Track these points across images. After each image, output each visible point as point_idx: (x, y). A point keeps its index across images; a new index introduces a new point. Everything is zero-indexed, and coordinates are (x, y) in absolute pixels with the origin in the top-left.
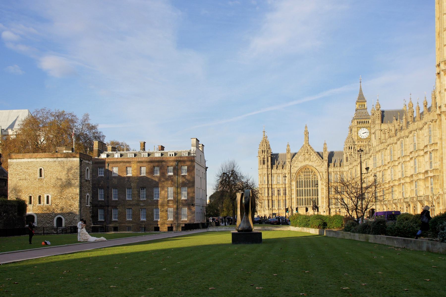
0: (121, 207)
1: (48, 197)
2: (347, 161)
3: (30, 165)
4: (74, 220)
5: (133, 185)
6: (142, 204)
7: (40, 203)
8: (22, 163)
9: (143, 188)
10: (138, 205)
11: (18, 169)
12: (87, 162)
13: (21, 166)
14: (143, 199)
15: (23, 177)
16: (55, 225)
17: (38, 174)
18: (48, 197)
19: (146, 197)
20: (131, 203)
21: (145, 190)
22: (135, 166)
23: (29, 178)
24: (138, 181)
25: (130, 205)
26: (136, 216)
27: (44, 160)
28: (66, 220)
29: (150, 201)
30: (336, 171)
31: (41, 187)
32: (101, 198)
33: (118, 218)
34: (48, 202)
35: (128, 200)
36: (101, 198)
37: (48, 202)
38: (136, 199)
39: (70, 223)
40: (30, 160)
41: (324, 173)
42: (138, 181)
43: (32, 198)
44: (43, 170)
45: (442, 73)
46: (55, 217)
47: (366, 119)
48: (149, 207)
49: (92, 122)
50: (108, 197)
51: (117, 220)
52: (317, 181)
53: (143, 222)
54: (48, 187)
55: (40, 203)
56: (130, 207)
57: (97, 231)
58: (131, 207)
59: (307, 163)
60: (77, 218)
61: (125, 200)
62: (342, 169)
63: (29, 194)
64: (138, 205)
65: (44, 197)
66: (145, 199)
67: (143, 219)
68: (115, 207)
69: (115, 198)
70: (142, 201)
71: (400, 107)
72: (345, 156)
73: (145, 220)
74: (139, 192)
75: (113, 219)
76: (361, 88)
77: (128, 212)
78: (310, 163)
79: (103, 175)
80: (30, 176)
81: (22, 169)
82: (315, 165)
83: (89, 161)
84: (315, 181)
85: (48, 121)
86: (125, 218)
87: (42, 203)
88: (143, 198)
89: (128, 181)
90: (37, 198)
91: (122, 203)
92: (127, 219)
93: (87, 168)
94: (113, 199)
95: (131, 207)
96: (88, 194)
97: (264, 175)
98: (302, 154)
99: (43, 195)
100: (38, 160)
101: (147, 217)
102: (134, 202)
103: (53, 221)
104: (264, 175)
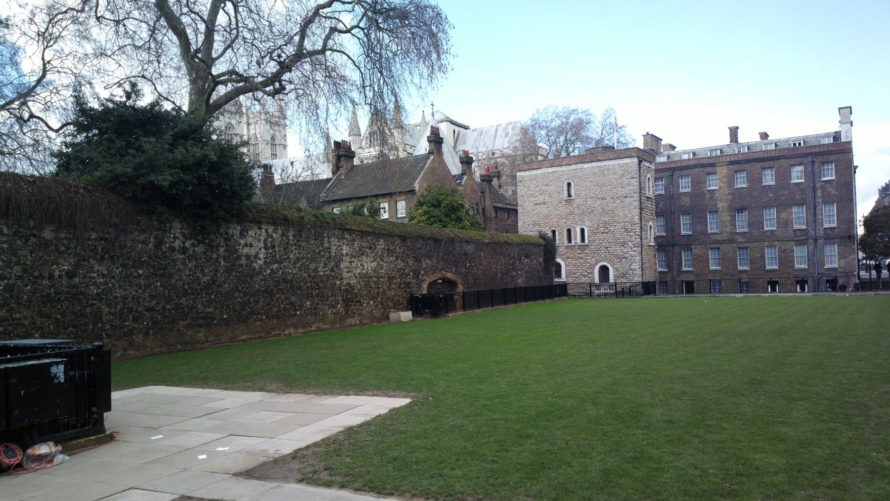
0: (698, 246)
1: (582, 230)
3: (551, 179)
5: (720, 205)
7: (570, 241)
8: (536, 176)
9: (740, 210)
10: (731, 241)
11: (532, 186)
12: (648, 165)
15: (540, 199)
16: (597, 280)
17: (566, 192)
18: (582, 230)
19: (749, 226)
20: (719, 238)
21: (746, 213)
24: (730, 197)
25: (716, 242)
27: (574, 167)
28: (616, 269)
29: (756, 233)
31: (571, 213)
33: (694, 266)
34: (583, 240)
37: (583, 240)
38: (728, 230)
39: (624, 275)
40: (550, 170)
42: (730, 197)
43: (557, 233)
48: (755, 244)
50: (673, 230)
53: (742, 272)
55: (570, 241)
56: (716, 246)
57: (654, 292)
58: (719, 246)
61: (705, 233)
64: (731, 241)
66: (746, 230)
67: (771, 265)
68: (687, 247)
69: (798, 178)
70: (740, 234)
73: (746, 268)
74: (733, 218)
75: (684, 269)
77: (712, 255)
79: (663, 192)
80: (550, 196)
83: (651, 163)
85: (553, 125)
86: (708, 266)
87: (573, 241)
88: (742, 224)
89: (711, 198)
90: (565, 233)
91: (700, 238)
92: (711, 268)
93: (649, 176)
94: (683, 232)
95: (719, 246)
96: (651, 223)
99: (574, 228)
100: (564, 168)
101: (752, 262)
102: (725, 236)
103: (592, 273)
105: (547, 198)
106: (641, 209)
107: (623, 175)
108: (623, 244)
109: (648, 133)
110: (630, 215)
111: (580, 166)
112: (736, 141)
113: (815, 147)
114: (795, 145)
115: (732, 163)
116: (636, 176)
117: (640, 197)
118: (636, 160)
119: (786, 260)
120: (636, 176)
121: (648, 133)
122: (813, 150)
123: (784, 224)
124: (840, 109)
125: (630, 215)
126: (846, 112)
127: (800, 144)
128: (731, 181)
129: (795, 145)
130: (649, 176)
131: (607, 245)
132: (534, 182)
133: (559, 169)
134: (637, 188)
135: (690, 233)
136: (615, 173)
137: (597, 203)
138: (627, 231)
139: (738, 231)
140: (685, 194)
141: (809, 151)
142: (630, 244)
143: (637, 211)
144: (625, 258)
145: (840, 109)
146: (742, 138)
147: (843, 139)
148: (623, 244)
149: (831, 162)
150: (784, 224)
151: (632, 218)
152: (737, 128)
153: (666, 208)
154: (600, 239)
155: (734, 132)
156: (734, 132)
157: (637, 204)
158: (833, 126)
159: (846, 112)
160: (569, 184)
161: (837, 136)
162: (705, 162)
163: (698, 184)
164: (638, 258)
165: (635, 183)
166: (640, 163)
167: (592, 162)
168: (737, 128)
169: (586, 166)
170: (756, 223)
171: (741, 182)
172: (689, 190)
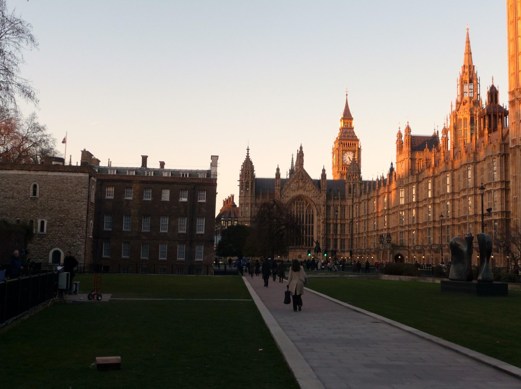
1: (43, 223)
2: (350, 192)
4: (77, 254)
5: (132, 211)
6: (144, 238)
8: (8, 175)
13: (8, 180)
14: (145, 230)
17: (32, 192)
22: (138, 187)
23: (18, 196)
26: (172, 254)
27: (40, 173)
30: (337, 205)
31: (35, 208)
32: (106, 228)
35: (125, 232)
36: (106, 228)
40: (20, 172)
41: (322, 207)
44: (38, 186)
45: (517, 102)
46: (51, 249)
47: (353, 140)
49: (41, 121)
51: (108, 256)
52: (313, 215)
53: (125, 259)
54: (43, 210)
59: (301, 192)
60: (81, 253)
62: (343, 203)
63: (16, 217)
65: (37, 223)
66: (148, 231)
67: (144, 257)
70: (144, 233)
71: (429, 133)
72: (347, 187)
74: (141, 221)
75: (104, 256)
76: (347, 100)
78: (305, 193)
80: (19, 193)
81: (8, 183)
82: (310, 195)
84: (310, 215)
88: (146, 227)
94: (105, 229)
97: (247, 204)
98: (295, 181)
100: (32, 173)
103: (48, 256)
104: (247, 204)
105: (15, 194)
106: (88, 211)
107: (77, 185)
108: (73, 236)
109: (85, 150)
110: (80, 215)
111: (45, 173)
112: (146, 166)
113: (195, 179)
114: (183, 175)
115: (143, 182)
116: (87, 186)
117: (88, 202)
118: (87, 175)
119: (172, 254)
120: (87, 186)
121: (85, 150)
122: (194, 181)
123: (173, 228)
124: (212, 156)
125: (80, 215)
126: (215, 159)
127: (186, 175)
128: (141, 195)
129: (183, 175)
130: (93, 187)
131: (61, 235)
132: (6, 180)
133: (27, 173)
134: (87, 195)
135: (110, 229)
136: (71, 182)
137: (56, 203)
138: (77, 227)
139: (143, 231)
140: (109, 200)
141: (192, 181)
142: (79, 236)
143: (85, 212)
144: (74, 246)
145: (212, 156)
146: (149, 165)
147: (212, 177)
148: (73, 236)
149: (204, 191)
150: (173, 228)
151: (82, 217)
152: (147, 157)
153: (100, 209)
154: (56, 231)
155: (144, 159)
156: (144, 159)
157: (85, 207)
158: (206, 166)
159: (215, 159)
160: (35, 186)
161: (208, 173)
162: (125, 178)
163: (119, 194)
164: (83, 247)
165: (85, 191)
166: (90, 177)
167: (55, 171)
168: (147, 157)
169: (50, 174)
170: (155, 227)
171: (148, 198)
172: (112, 197)
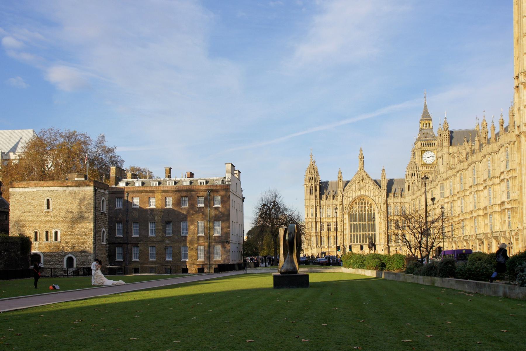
0: (143, 245)
1: (56, 233)
2: (409, 190)
3: (35, 195)
4: (87, 259)
5: (156, 218)
6: (167, 242)
7: (47, 240)
8: (25, 192)
9: (169, 222)
10: (162, 242)
11: (21, 199)
12: (103, 191)
13: (25, 197)
14: (168, 235)
15: (27, 209)
16: (65, 266)
17: (45, 206)
18: (56, 233)
19: (173, 233)
20: (155, 240)
21: (171, 225)
22: (160, 197)
23: (34, 210)
24: (163, 213)
25: (153, 242)
26: (160, 255)
27: (52, 189)
28: (78, 260)
29: (176, 237)
30: (397, 203)
31: (49, 221)
32: (119, 234)
33: (139, 258)
34: (56, 239)
35: (151, 237)
36: (119, 234)
37: (56, 239)
38: (160, 235)
39: (83, 263)
40: (35, 189)
41: (382, 205)
42: (163, 213)
43: (38, 234)
44: (50, 200)
45: (521, 86)
46: (65, 256)
47: (432, 140)
48: (176, 244)
49: (109, 144)
50: (127, 233)
51: (138, 260)
52: (374, 214)
53: (168, 262)
54: (57, 221)
55: (47, 240)
56: (153, 245)
57: (115, 273)
58: (155, 245)
59: (362, 192)
60: (91, 258)
61: (147, 236)
62: (403, 200)
63: (34, 229)
64: (162, 242)
65: (51, 233)
66: (171, 235)
67: (169, 259)
68: (136, 245)
70: (167, 238)
71: (472, 126)
72: (406, 185)
73: (171, 260)
74: (164, 227)
75: (134, 259)
76: (425, 104)
77: (151, 251)
78: (366, 193)
79: (122, 207)
80: (35, 208)
81: (25, 200)
82: (371, 195)
83: (105, 190)
84: (371, 214)
85: (57, 143)
86: (148, 258)
87: (50, 240)
88: (169, 234)
89: (151, 213)
90: (44, 234)
91: (144, 240)
92: (150, 259)
93: (103, 198)
94: (134, 235)
95: (155, 245)
96: (104, 229)
97: (312, 207)
98: (356, 182)
99: (51, 230)
100: (45, 189)
101: (173, 256)
102: (159, 239)
103: (62, 262)
104: (312, 207)
